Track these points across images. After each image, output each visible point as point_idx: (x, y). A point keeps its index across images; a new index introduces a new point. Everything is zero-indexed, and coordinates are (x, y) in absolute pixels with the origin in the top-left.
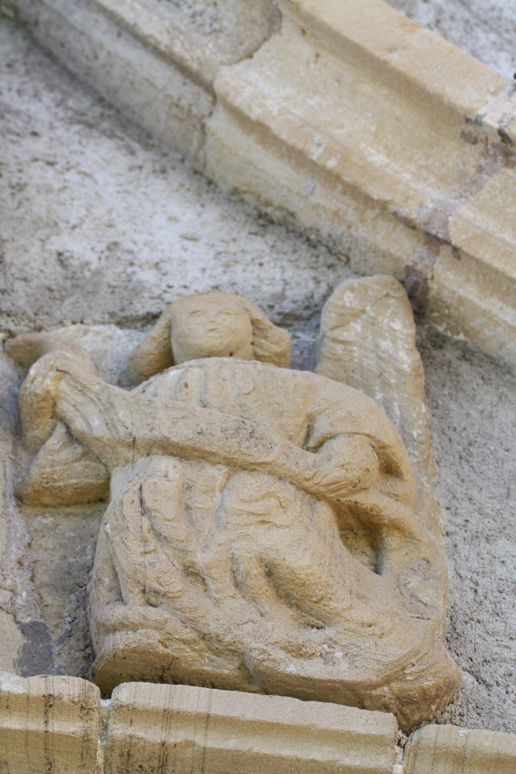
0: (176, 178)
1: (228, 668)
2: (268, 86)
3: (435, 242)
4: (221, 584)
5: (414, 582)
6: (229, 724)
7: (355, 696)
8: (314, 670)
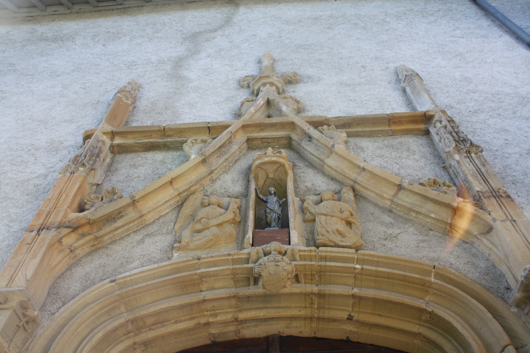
0: (320, 174)
1: (333, 244)
2: (331, 162)
3: (355, 182)
4: (331, 233)
5: (356, 230)
6: (334, 252)
7: (350, 247)
8: (344, 244)
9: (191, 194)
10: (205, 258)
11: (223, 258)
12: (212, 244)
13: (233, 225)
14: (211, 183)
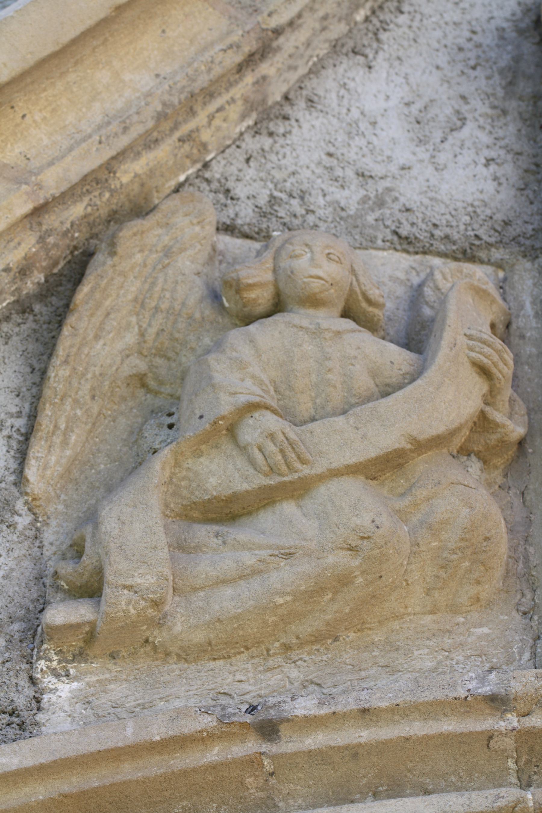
9: (116, 218)
10: (311, 723)
11: (449, 726)
12: (337, 611)
13: (475, 466)
14: (256, 130)
